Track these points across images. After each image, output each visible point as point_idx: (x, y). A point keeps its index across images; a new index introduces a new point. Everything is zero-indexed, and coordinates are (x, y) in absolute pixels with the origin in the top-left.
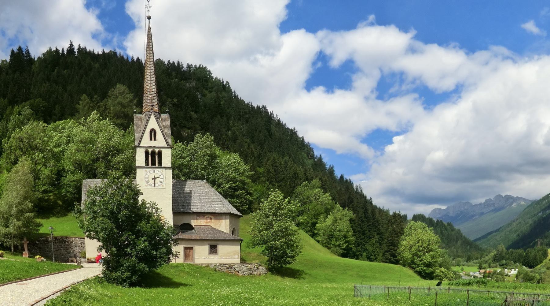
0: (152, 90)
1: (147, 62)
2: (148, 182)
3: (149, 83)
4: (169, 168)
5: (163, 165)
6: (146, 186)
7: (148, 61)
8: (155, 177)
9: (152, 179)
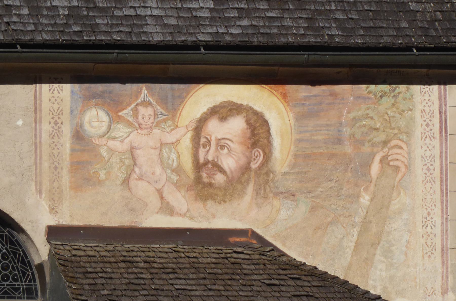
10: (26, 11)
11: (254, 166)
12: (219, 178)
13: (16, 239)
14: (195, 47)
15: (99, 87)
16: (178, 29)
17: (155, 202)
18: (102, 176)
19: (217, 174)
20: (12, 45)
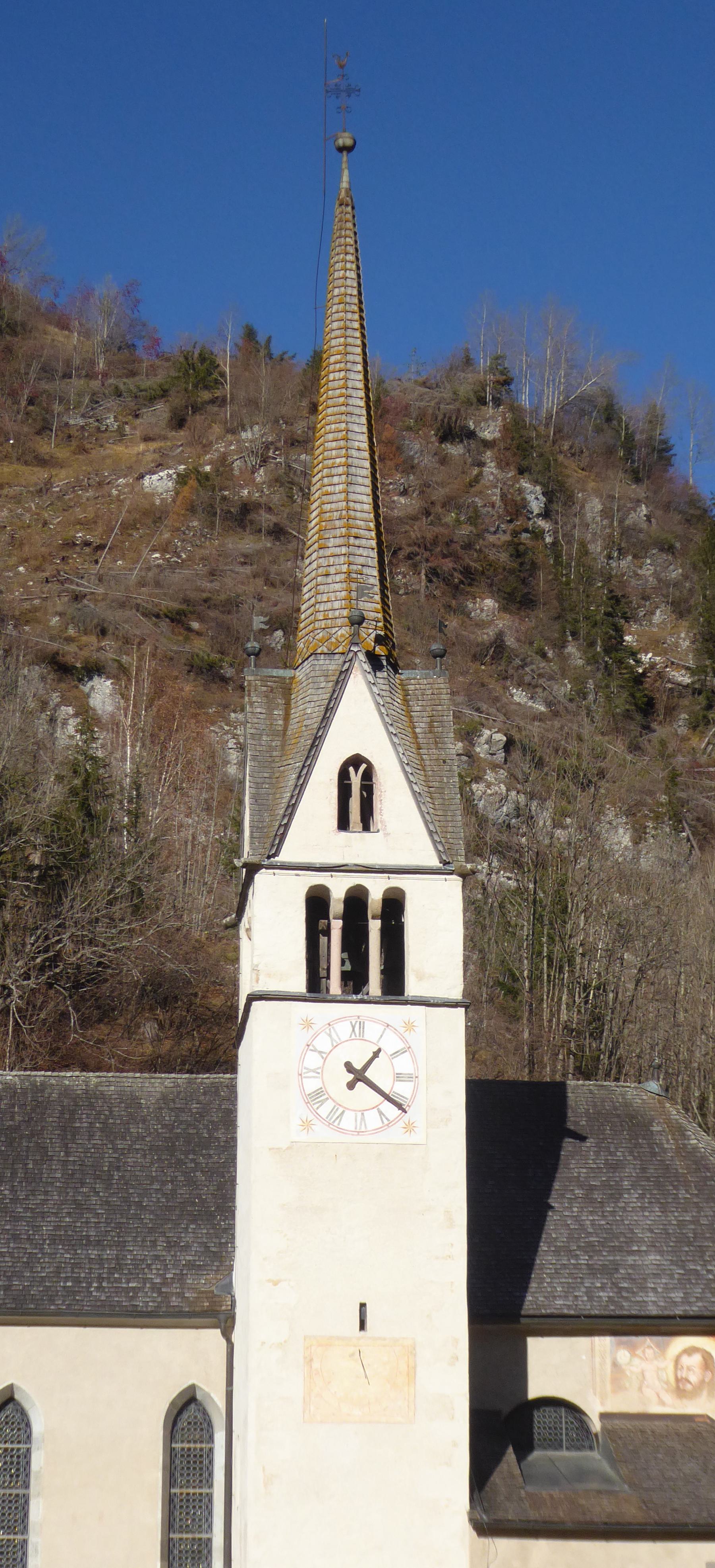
0: (354, 531)
1: (331, 377)
2: (318, 1096)
3: (341, 470)
4: (454, 1005)
5: (413, 987)
6: (307, 1125)
7: (338, 333)
8: (358, 1066)
9: (351, 1086)
10: (585, 1298)
11: (707, 1380)
12: (689, 1387)
13: (561, 1446)
14: (673, 1317)
15: (624, 1339)
16: (665, 1308)
17: (655, 1399)
18: (627, 1385)
19: (92, 688)
20: (578, 1317)
